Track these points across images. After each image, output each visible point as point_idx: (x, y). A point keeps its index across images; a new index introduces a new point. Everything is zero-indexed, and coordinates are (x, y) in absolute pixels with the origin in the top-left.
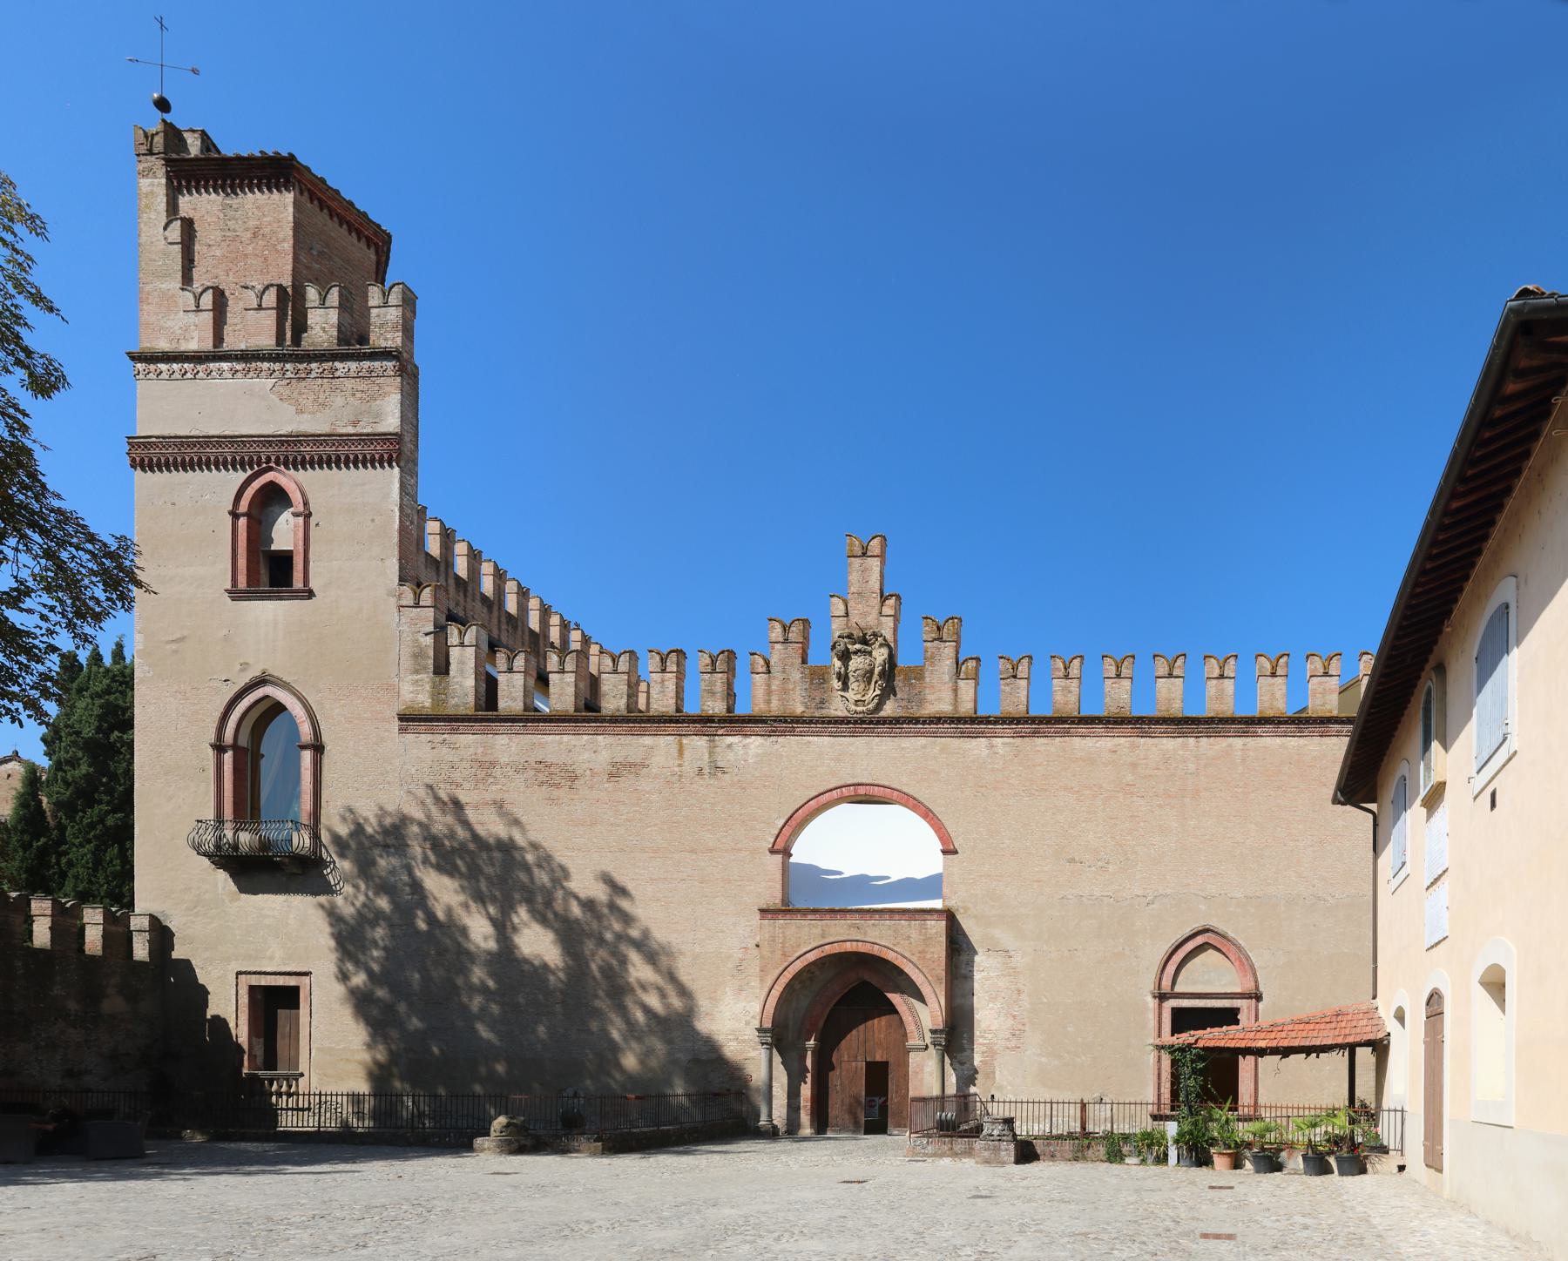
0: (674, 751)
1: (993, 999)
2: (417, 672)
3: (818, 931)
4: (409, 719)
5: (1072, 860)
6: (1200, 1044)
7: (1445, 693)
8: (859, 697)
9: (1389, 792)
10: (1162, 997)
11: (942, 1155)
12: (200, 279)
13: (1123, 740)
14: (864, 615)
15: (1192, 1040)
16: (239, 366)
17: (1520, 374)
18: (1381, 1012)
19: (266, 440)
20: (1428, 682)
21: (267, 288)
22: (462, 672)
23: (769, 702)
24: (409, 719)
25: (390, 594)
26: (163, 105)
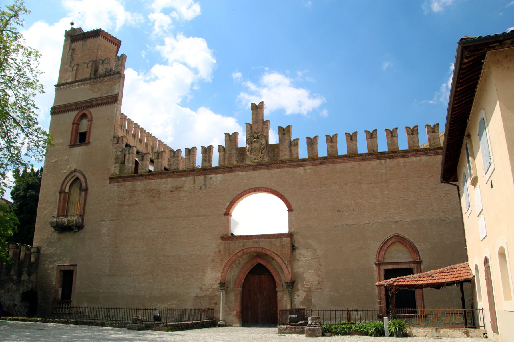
0: (192, 182)
1: (310, 269)
2: (116, 163)
3: (242, 244)
4: (113, 179)
5: (339, 211)
6: (395, 284)
7: (471, 144)
8: (256, 157)
9: (461, 178)
10: (378, 265)
11: (292, 333)
12: (75, 63)
13: (355, 163)
14: (257, 129)
15: (392, 282)
16: (80, 83)
17: (467, 58)
18: (471, 267)
19: (84, 102)
20: (466, 141)
21: (90, 62)
22: (129, 162)
23: (224, 162)
24: (113, 179)
25: (111, 140)
26: (72, 24)
